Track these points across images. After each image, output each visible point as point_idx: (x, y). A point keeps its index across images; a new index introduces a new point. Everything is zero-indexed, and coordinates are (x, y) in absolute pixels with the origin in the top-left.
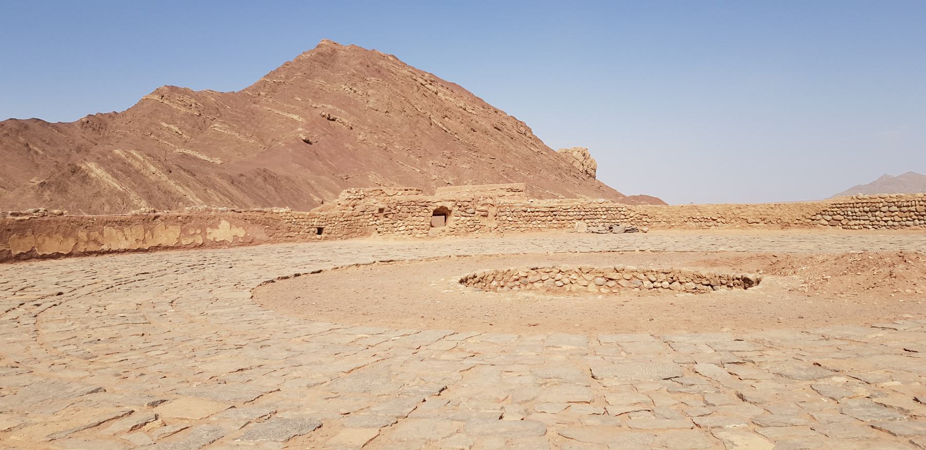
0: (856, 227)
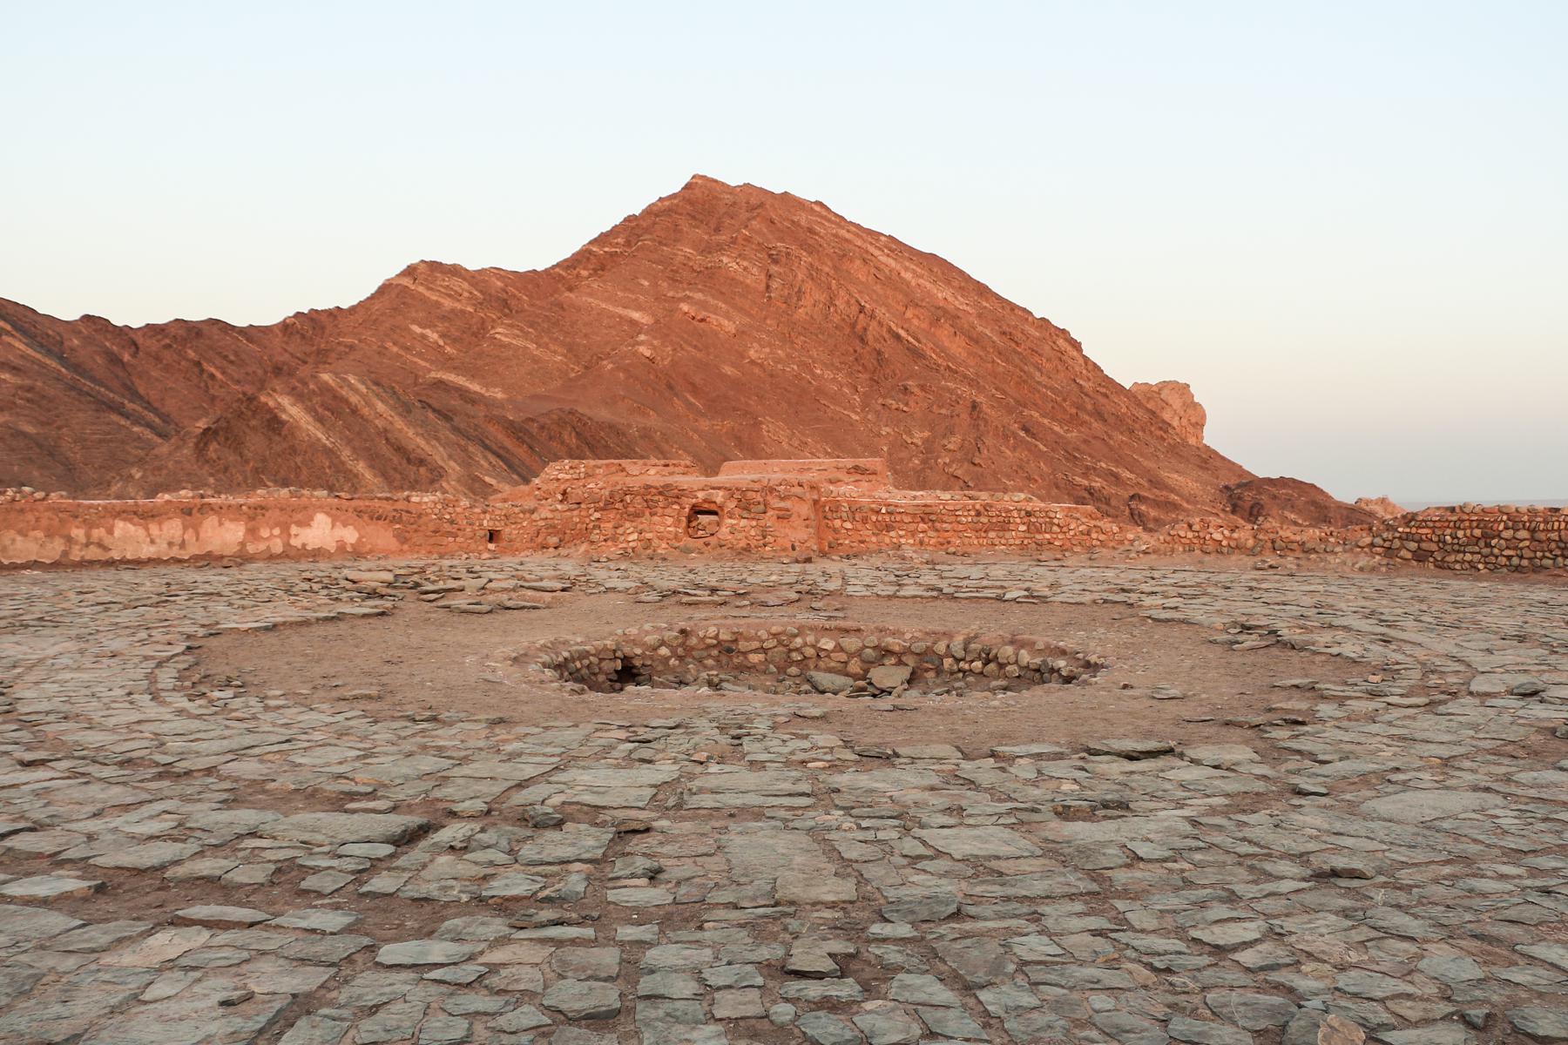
0: (1458, 566)
